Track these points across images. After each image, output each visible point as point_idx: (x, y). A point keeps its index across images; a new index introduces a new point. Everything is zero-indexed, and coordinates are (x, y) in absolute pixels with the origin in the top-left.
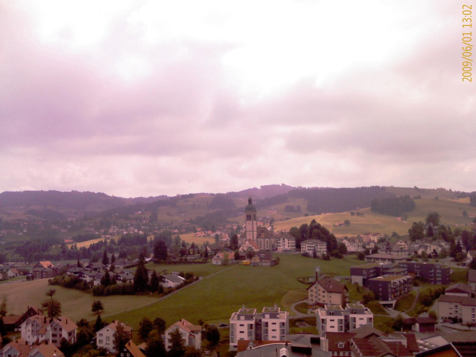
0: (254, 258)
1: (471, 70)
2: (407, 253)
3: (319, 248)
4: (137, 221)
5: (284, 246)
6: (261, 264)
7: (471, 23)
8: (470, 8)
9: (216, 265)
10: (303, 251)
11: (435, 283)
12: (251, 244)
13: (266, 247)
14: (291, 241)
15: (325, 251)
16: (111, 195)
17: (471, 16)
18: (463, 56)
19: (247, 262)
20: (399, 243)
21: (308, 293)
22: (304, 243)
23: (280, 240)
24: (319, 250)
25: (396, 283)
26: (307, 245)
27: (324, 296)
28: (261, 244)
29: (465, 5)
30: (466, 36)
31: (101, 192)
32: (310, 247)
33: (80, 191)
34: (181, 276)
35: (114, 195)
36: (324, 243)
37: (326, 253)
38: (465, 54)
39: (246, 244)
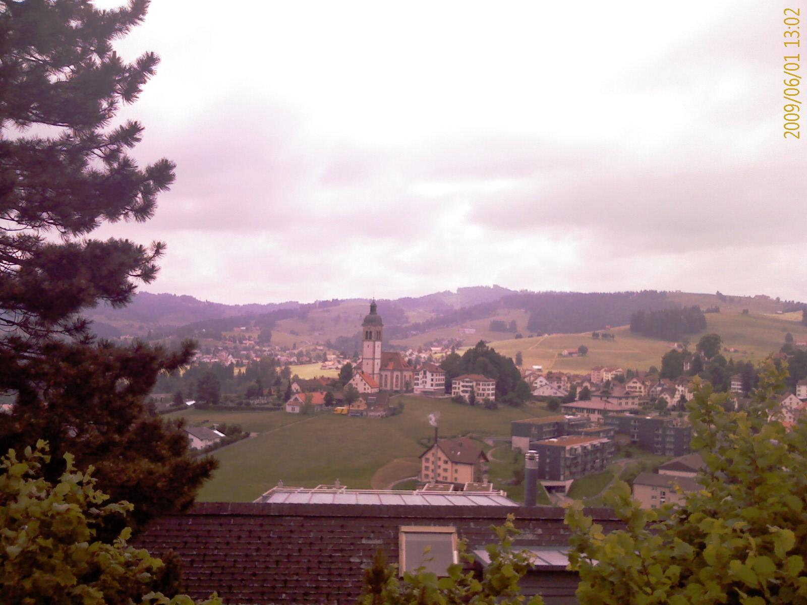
0: (355, 404)
1: (798, 119)
2: (637, 401)
3: (481, 389)
4: (235, 342)
5: (424, 384)
6: (367, 414)
7: (799, 39)
8: (796, 13)
9: (290, 413)
10: (456, 394)
11: (664, 454)
12: (363, 380)
13: (394, 386)
14: (437, 376)
15: (492, 395)
16: (203, 300)
17: (798, 28)
18: (785, 96)
19: (343, 409)
20: (631, 384)
21: (421, 462)
22: (457, 380)
23: (418, 375)
24: (481, 392)
25: (576, 449)
26: (462, 384)
27: (445, 470)
28: (386, 381)
29: (788, 9)
30: (789, 60)
31: (188, 294)
32: (467, 387)
33: (152, 293)
34: (220, 431)
35: (208, 301)
36: (491, 381)
37: (492, 398)
38: (788, 92)
39: (355, 380)
